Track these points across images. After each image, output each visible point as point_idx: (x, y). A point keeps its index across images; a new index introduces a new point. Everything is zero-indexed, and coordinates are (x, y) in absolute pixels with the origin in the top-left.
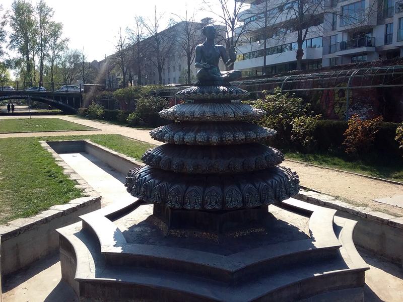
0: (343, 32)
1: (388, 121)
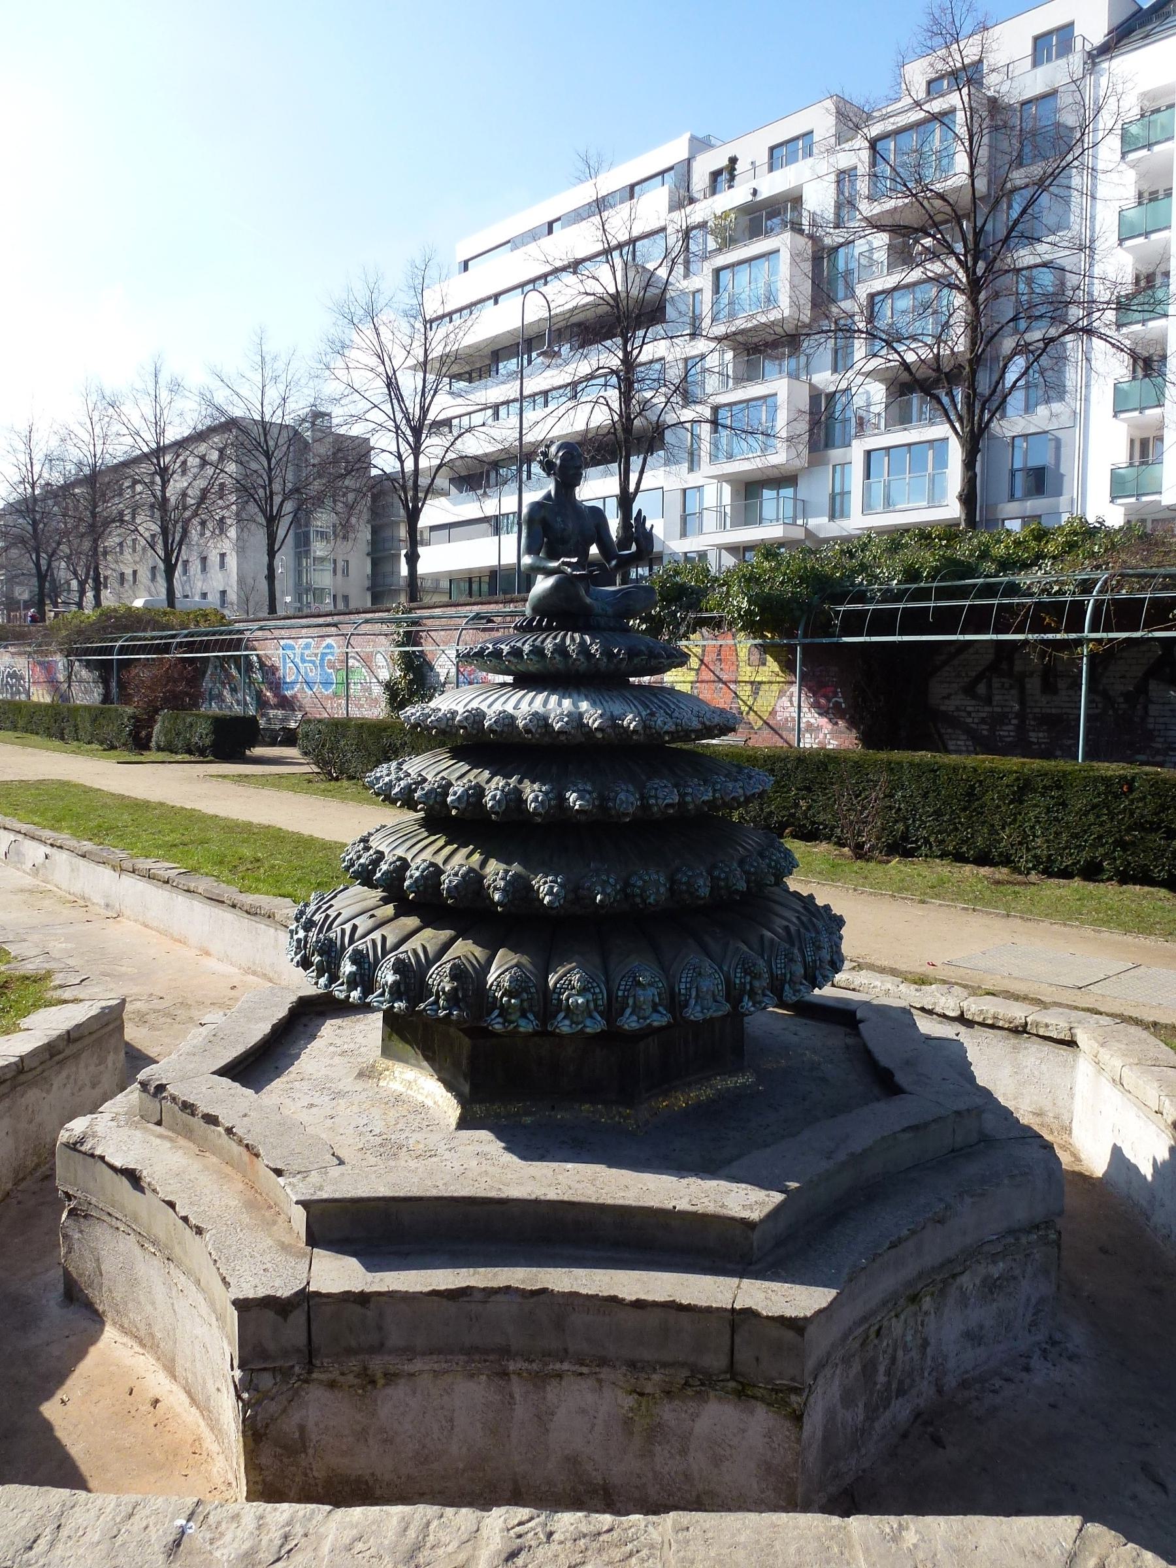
0: (721, 478)
1: (684, 751)
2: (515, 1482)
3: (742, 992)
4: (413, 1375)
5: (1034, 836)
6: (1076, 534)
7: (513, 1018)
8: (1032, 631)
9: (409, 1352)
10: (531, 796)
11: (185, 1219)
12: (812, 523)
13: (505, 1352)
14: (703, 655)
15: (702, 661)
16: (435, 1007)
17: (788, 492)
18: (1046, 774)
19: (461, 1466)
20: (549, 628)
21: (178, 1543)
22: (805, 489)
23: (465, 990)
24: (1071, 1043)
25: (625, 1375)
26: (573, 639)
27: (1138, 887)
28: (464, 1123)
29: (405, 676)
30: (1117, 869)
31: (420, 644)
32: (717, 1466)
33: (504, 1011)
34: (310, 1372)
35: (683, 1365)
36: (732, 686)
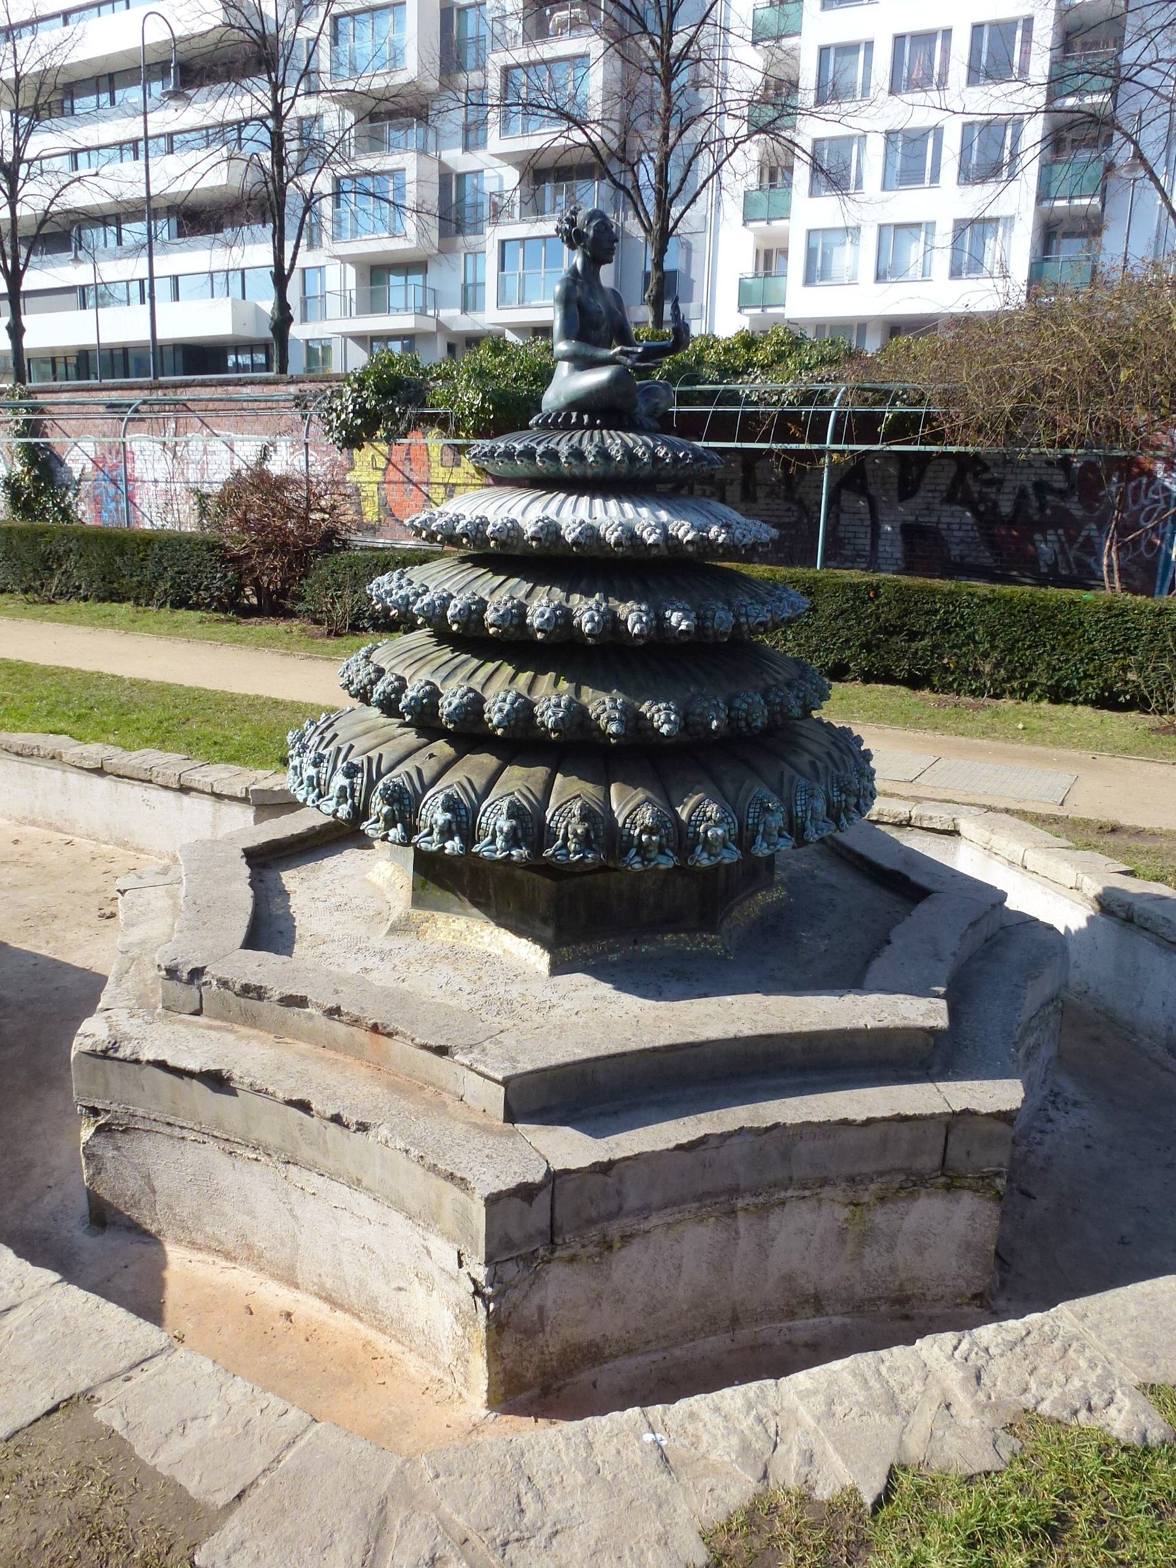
2: (734, 1310)
3: (839, 810)
4: (649, 1232)
5: (786, 640)
6: (782, 343)
7: (653, 855)
8: (776, 441)
9: (645, 1211)
10: (587, 616)
11: (336, 1119)
12: (445, 314)
13: (735, 1191)
14: (391, 454)
15: (389, 460)
16: (564, 851)
17: (416, 279)
18: (798, 581)
19: (685, 1307)
20: (592, 426)
21: (664, 1458)
22: (435, 277)
23: (596, 831)
24: (954, 833)
25: (844, 1191)
26: (591, 439)
27: (881, 686)
28: (557, 969)
29: (29, 472)
30: (862, 669)
31: (45, 435)
32: (921, 1254)
33: (642, 849)
34: (552, 1252)
35: (900, 1170)
36: (424, 488)
